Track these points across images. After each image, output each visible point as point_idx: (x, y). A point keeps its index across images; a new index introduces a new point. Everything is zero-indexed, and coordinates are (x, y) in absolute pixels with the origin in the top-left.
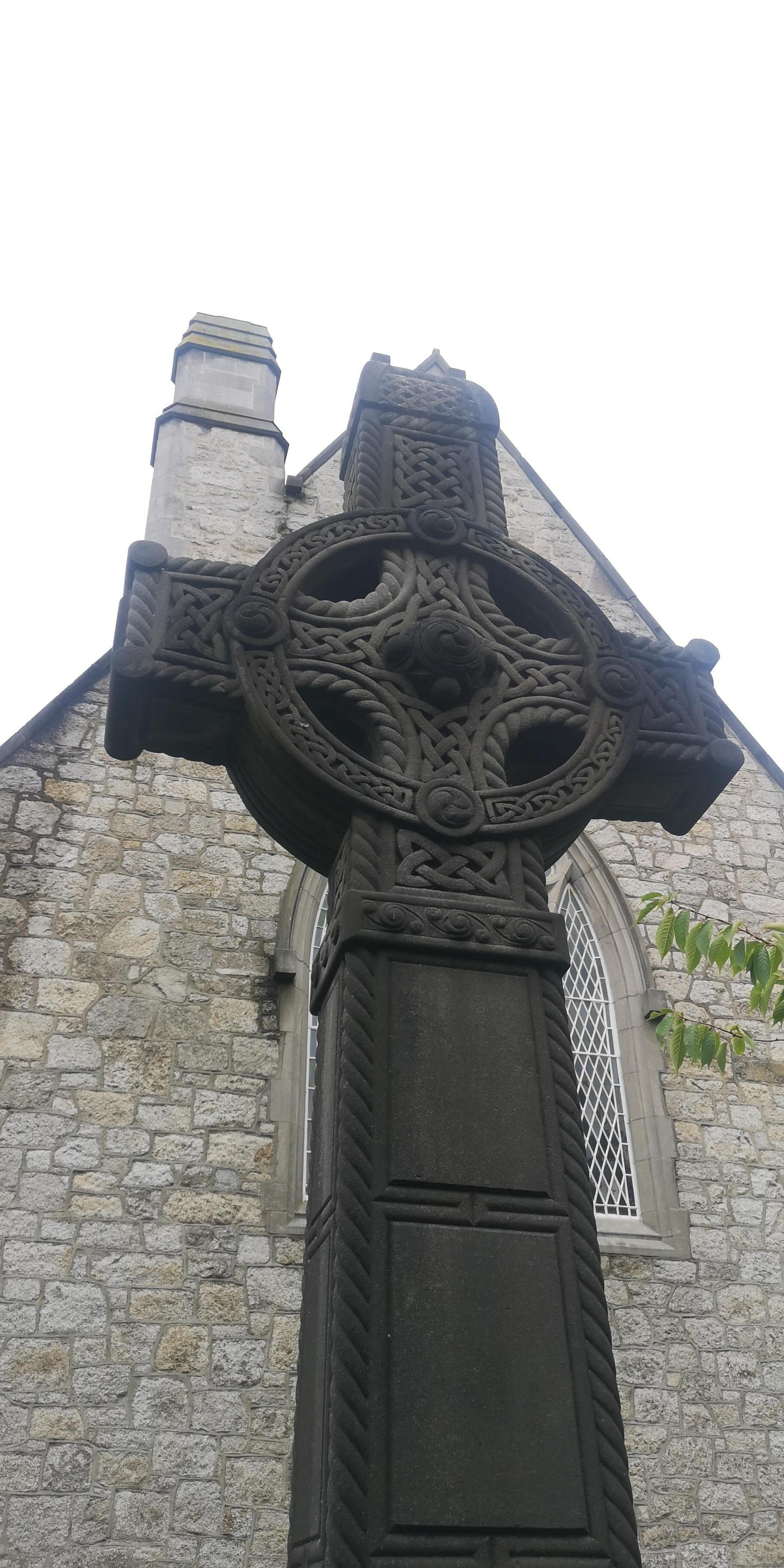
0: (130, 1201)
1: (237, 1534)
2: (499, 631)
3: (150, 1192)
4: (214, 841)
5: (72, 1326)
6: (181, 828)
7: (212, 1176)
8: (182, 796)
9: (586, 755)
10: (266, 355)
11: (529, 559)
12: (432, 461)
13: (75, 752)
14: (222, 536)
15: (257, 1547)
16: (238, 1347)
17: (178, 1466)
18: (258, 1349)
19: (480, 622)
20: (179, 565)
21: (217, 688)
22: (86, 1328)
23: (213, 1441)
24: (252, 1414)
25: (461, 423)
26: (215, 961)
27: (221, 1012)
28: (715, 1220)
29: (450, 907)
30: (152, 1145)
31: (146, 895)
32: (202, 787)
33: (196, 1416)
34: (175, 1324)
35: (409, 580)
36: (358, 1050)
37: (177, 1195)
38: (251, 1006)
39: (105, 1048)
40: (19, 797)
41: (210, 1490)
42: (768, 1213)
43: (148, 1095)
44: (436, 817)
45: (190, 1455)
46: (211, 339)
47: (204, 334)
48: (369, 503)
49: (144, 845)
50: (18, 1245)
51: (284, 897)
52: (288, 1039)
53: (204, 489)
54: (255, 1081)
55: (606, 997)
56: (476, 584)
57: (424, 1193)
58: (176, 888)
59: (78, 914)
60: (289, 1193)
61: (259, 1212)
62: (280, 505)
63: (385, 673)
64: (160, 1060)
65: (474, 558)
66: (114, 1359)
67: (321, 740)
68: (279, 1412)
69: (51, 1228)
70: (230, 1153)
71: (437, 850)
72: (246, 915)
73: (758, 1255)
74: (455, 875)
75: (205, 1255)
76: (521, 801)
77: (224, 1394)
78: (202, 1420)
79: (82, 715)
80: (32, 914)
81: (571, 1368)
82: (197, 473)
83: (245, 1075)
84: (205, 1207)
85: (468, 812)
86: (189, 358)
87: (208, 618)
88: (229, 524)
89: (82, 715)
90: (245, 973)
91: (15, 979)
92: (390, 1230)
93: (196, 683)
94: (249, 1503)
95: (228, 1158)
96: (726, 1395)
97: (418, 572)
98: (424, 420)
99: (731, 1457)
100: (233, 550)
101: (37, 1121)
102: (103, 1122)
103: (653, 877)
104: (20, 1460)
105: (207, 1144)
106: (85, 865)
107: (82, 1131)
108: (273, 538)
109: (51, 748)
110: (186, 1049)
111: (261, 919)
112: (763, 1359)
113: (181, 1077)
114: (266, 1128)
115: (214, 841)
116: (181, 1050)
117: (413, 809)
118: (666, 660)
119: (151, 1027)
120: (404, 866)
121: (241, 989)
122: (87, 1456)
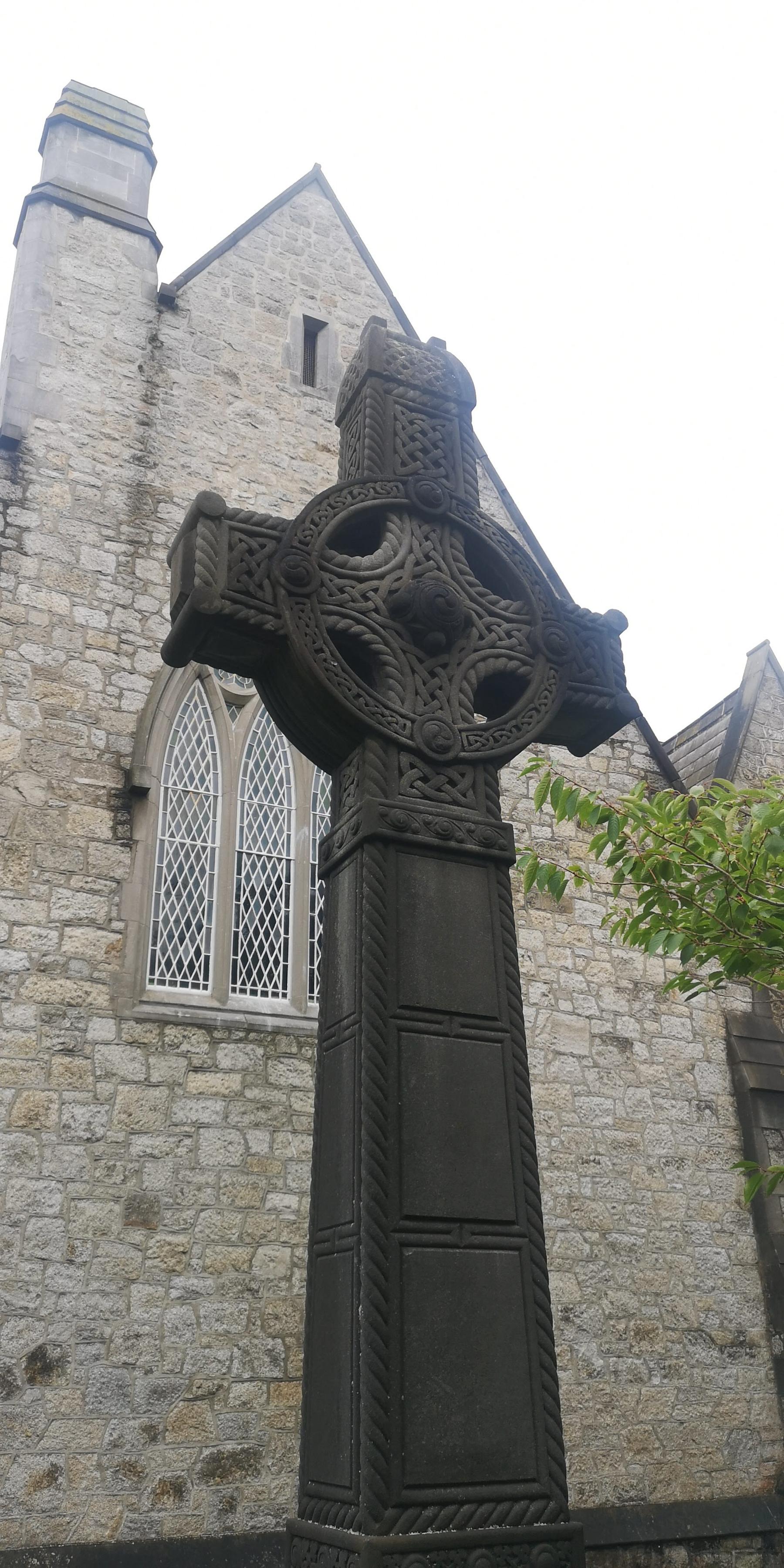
1: (78, 1260)
2: (472, 591)
3: (8, 975)
4: (76, 655)
6: (43, 640)
7: (65, 964)
9: (532, 701)
10: (143, 141)
12: (423, 433)
14: (91, 340)
15: (95, 1270)
16: (84, 1109)
17: (29, 1205)
18: (103, 1112)
19: (458, 582)
20: (234, 515)
21: (268, 626)
23: (60, 1186)
24: (95, 1164)
25: (447, 399)
26: (73, 770)
27: (78, 818)
29: (438, 815)
30: (10, 933)
31: (8, 702)
34: (29, 1089)
35: (406, 541)
36: (376, 915)
37: (33, 979)
38: (106, 816)
41: (57, 1225)
42: (540, 1017)
43: (7, 889)
45: (39, 1197)
46: (85, 114)
47: (78, 107)
48: (376, 469)
49: (7, 652)
51: (142, 716)
52: (140, 847)
53: (73, 284)
54: (108, 883)
56: (456, 549)
57: (421, 1015)
58: (38, 698)
60: (135, 982)
61: (107, 997)
62: (152, 314)
63: (390, 622)
64: (20, 859)
65: (455, 526)
67: (347, 677)
68: (118, 1164)
70: (83, 945)
71: (427, 770)
72: (104, 729)
74: (439, 790)
75: (58, 1032)
76: (486, 734)
77: (71, 1148)
78: (51, 1168)
81: (509, 1126)
82: (67, 265)
83: (99, 877)
84: (59, 991)
85: (450, 742)
86: (61, 131)
87: (259, 565)
88: (99, 327)
90: (101, 784)
92: (399, 1038)
93: (252, 621)
94: (90, 1235)
95: (81, 950)
97: (413, 534)
98: (418, 393)
100: (102, 356)
105: (61, 936)
108: (143, 349)
110: (44, 849)
111: (118, 734)
113: (39, 874)
114: (117, 925)
115: (76, 655)
116: (39, 850)
117: (411, 737)
118: (590, 625)
119: (11, 827)
120: (404, 781)
121: (98, 798)
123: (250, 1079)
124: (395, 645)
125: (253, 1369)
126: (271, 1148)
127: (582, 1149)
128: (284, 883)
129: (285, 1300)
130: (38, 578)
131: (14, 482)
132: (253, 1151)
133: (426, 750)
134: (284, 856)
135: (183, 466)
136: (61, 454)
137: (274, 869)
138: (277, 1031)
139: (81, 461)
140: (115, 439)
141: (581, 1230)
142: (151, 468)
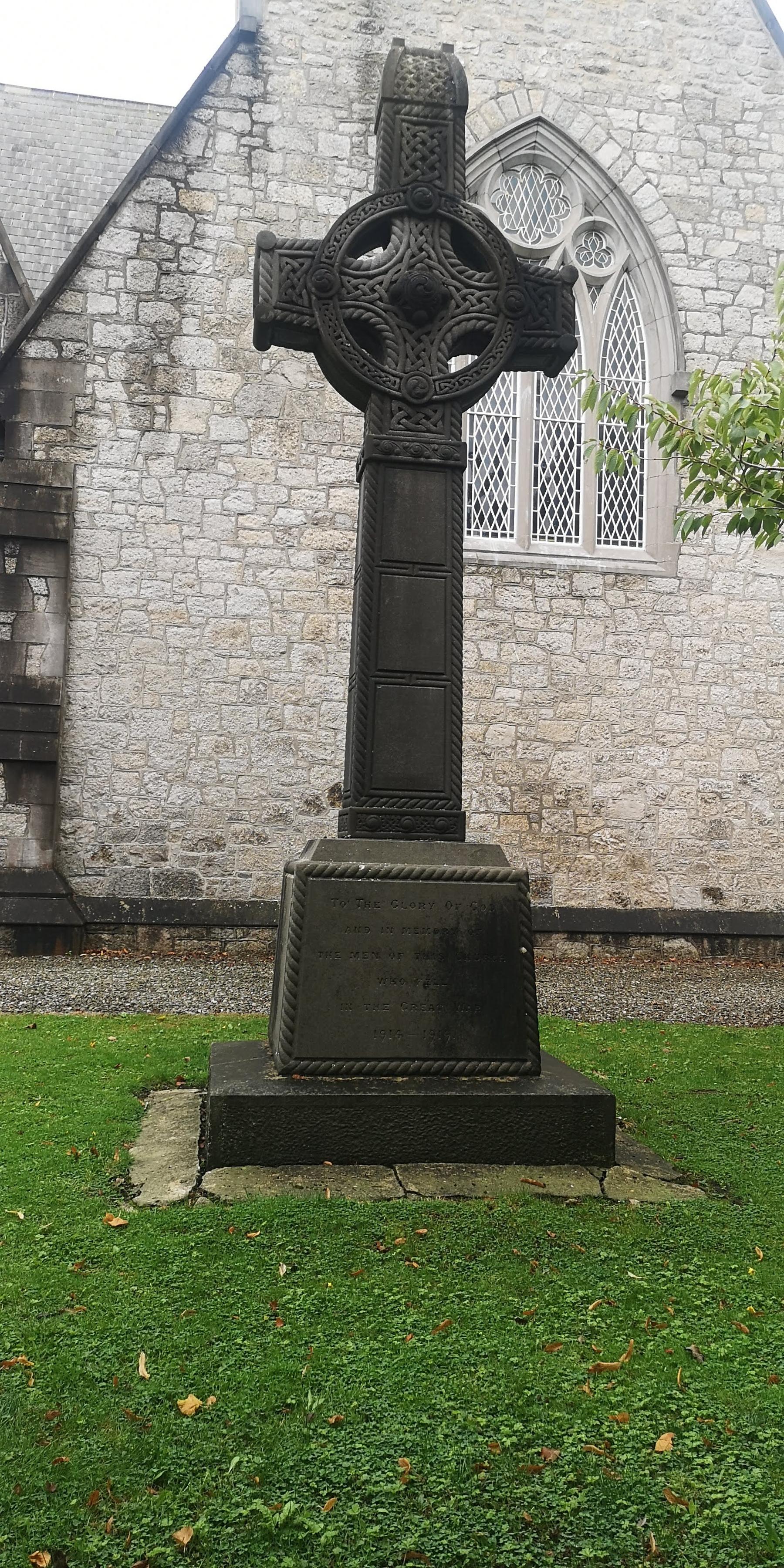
0: (278, 534)
2: (453, 271)
5: (248, 612)
8: (292, 202)
11: (475, 217)
13: (200, 161)
22: (257, 613)
28: (700, 550)
29: (413, 441)
30: (289, 496)
32: (308, 192)
33: (330, 666)
35: (405, 240)
37: (310, 531)
39: (250, 425)
40: (160, 209)
44: (410, 394)
50: (207, 561)
55: (644, 378)
57: (395, 564)
59: (219, 316)
63: (390, 306)
66: (276, 632)
69: (226, 551)
71: (410, 410)
73: (728, 574)
79: (201, 121)
80: (184, 316)
89: (201, 121)
91: (178, 370)
95: (343, 506)
96: (685, 664)
98: (421, 107)
99: (681, 700)
101: (208, 479)
102: (255, 480)
103: (701, 265)
104: (224, 686)
105: (328, 495)
106: (220, 271)
107: (240, 486)
109: (180, 158)
110: (309, 425)
112: (717, 642)
117: (399, 390)
119: (282, 409)
120: (394, 420)
122: (265, 685)
123: (481, 603)
124: (393, 323)
125: (487, 806)
126: (499, 655)
127: (773, 654)
128: (511, 439)
129: (511, 761)
130: (283, 173)
131: (256, 77)
132: (484, 657)
133: (408, 398)
134: (511, 415)
135: (408, 24)
136: (294, 36)
137: (502, 427)
138: (503, 565)
139: (313, 41)
140: (342, 9)
141: (765, 717)
142: (377, 34)
